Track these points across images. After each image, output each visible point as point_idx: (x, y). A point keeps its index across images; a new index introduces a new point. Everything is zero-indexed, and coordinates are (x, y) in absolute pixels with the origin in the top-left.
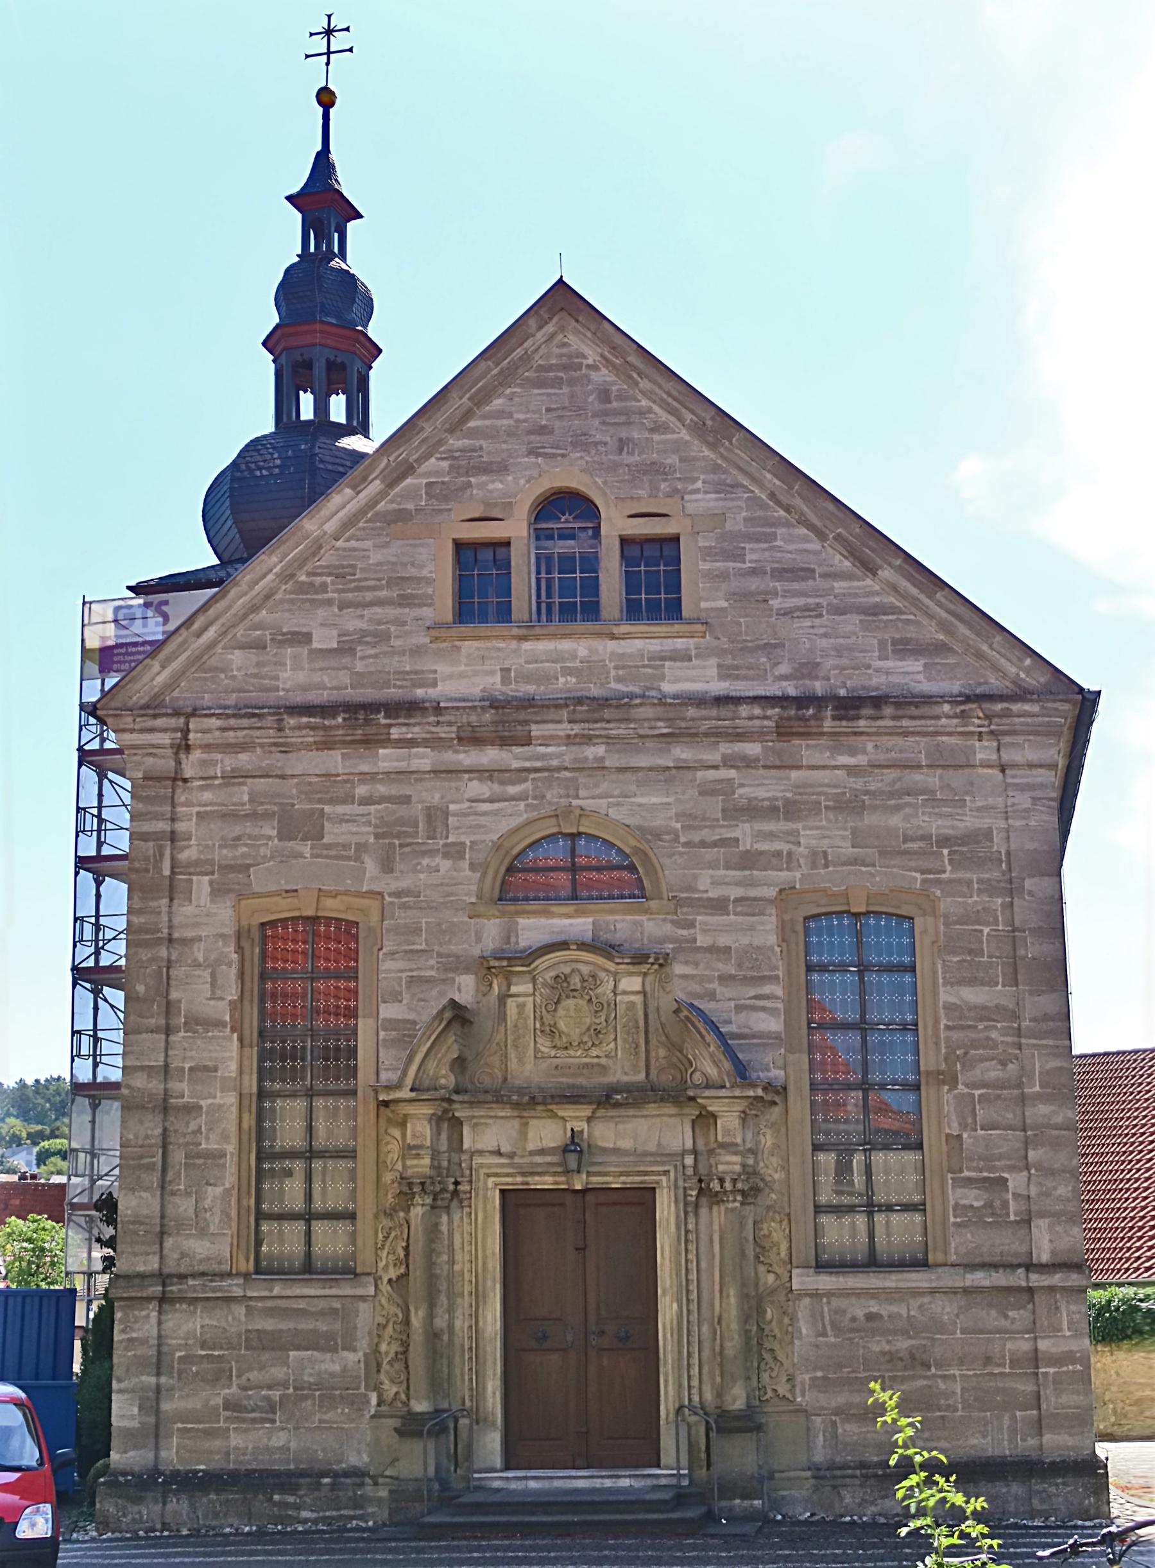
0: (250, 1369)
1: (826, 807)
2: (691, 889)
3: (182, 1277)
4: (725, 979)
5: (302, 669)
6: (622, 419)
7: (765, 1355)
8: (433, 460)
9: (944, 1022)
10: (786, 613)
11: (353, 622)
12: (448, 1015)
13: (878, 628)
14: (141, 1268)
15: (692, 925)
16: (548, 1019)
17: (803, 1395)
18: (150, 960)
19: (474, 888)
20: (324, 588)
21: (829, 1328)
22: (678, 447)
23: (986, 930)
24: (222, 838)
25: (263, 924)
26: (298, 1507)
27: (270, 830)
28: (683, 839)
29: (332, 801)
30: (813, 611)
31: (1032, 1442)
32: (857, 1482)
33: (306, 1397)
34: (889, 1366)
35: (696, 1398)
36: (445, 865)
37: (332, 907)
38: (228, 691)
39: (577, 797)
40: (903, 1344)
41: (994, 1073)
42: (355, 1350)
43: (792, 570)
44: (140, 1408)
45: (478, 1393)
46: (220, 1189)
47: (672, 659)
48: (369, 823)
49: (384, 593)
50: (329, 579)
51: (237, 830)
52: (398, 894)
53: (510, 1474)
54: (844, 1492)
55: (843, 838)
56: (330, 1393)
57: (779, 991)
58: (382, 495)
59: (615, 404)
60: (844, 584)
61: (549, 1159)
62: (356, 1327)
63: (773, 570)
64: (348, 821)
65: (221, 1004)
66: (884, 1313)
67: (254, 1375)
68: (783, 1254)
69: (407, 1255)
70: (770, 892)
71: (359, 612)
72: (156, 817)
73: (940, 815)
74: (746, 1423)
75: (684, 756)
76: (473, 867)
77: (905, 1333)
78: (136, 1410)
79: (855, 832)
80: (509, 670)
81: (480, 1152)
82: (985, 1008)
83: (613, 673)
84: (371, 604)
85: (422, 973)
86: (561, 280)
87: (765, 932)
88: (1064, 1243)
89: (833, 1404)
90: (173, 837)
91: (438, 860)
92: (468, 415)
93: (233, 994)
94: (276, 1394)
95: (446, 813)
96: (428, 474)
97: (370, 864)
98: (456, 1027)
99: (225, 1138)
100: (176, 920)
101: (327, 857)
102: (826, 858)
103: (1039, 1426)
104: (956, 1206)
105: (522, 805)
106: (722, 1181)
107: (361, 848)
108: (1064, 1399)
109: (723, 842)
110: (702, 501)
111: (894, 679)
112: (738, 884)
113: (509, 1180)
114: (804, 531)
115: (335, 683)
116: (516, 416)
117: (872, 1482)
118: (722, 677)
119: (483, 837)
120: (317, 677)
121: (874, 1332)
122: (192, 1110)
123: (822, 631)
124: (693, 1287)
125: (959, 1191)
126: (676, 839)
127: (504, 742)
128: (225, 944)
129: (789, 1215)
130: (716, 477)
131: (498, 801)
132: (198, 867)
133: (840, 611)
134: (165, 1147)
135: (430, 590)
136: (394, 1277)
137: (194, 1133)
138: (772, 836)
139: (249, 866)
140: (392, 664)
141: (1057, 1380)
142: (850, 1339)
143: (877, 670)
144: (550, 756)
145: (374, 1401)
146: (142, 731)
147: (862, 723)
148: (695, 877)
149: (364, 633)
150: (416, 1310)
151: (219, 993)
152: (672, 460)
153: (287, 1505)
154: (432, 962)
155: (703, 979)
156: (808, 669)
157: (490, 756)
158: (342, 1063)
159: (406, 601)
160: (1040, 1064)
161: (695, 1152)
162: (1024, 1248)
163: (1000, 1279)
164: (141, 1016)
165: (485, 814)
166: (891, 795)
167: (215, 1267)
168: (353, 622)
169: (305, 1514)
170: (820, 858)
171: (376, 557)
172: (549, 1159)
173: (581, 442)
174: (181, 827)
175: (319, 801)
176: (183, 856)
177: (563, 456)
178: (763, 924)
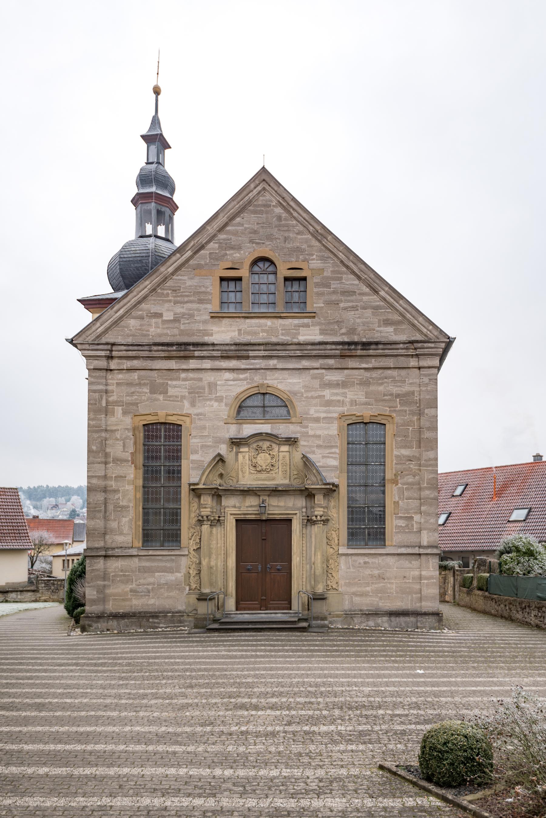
0: (140, 579)
2: (307, 414)
3: (113, 549)
4: (319, 446)
5: (159, 328)
6: (286, 228)
8: (212, 243)
9: (395, 462)
10: (345, 309)
11: (179, 309)
12: (218, 459)
13: (378, 315)
14: (97, 546)
15: (307, 427)
16: (254, 460)
18: (98, 437)
19: (226, 413)
20: (168, 295)
22: (307, 241)
23: (411, 428)
24: (127, 393)
25: (144, 425)
26: (159, 623)
27: (146, 390)
28: (305, 396)
29: (171, 380)
30: (355, 308)
31: (418, 605)
33: (162, 588)
35: (304, 589)
36: (216, 404)
37: (172, 419)
38: (128, 336)
39: (266, 379)
40: (376, 572)
41: (410, 479)
43: (348, 292)
44: (97, 592)
45: (226, 586)
46: (127, 519)
47: (303, 326)
48: (186, 388)
49: (192, 298)
50: (170, 292)
51: (133, 389)
52: (197, 415)
53: (238, 612)
54: (355, 619)
56: (170, 586)
57: (337, 451)
58: (191, 257)
59: (283, 222)
60: (367, 298)
61: (254, 509)
63: (341, 292)
65: (127, 454)
67: (142, 581)
68: (336, 541)
70: (336, 415)
71: (182, 305)
72: (99, 384)
73: (397, 386)
74: (321, 598)
75: (306, 364)
77: (377, 568)
78: (95, 593)
79: (367, 393)
80: (241, 330)
81: (228, 507)
82: (409, 457)
83: (280, 332)
84: (187, 302)
86: (263, 167)
87: (333, 429)
88: (432, 539)
90: (106, 392)
91: (213, 402)
92: (226, 225)
93: (132, 450)
94: (150, 587)
95: (216, 385)
96: (210, 249)
97: (186, 404)
98: (220, 463)
99: (130, 501)
100: (109, 423)
101: (169, 400)
103: (421, 600)
104: (396, 526)
105: (245, 382)
106: (316, 517)
107: (183, 397)
108: (429, 591)
110: (315, 264)
111: (383, 334)
112: (325, 412)
114: (352, 276)
115: (172, 333)
116: (245, 226)
118: (321, 334)
120: (165, 331)
122: (116, 491)
123: (358, 316)
124: (304, 552)
125: (397, 521)
126: (302, 396)
127: (239, 358)
128: (129, 432)
130: (321, 254)
131: (236, 380)
132: (117, 403)
133: (364, 308)
134: (105, 504)
135: (210, 297)
137: (117, 499)
138: (337, 394)
139: (138, 403)
140: (195, 327)
141: (427, 585)
143: (377, 331)
144: (256, 364)
145: (187, 588)
146: (92, 350)
147: (371, 351)
149: (184, 314)
151: (126, 450)
152: (304, 246)
153: (155, 623)
154: (210, 440)
155: (310, 447)
156: (352, 331)
157: (233, 364)
158: (176, 475)
159: (201, 301)
160: (427, 476)
161: (306, 507)
162: (418, 540)
163: (410, 551)
164: (94, 457)
165: (231, 385)
166: (380, 379)
167: (126, 545)
168: (179, 309)
169: (161, 625)
170: (353, 403)
171: (189, 283)
172: (254, 509)
173: (270, 237)
174: (110, 388)
175: (166, 379)
176: (111, 399)
177: (263, 243)
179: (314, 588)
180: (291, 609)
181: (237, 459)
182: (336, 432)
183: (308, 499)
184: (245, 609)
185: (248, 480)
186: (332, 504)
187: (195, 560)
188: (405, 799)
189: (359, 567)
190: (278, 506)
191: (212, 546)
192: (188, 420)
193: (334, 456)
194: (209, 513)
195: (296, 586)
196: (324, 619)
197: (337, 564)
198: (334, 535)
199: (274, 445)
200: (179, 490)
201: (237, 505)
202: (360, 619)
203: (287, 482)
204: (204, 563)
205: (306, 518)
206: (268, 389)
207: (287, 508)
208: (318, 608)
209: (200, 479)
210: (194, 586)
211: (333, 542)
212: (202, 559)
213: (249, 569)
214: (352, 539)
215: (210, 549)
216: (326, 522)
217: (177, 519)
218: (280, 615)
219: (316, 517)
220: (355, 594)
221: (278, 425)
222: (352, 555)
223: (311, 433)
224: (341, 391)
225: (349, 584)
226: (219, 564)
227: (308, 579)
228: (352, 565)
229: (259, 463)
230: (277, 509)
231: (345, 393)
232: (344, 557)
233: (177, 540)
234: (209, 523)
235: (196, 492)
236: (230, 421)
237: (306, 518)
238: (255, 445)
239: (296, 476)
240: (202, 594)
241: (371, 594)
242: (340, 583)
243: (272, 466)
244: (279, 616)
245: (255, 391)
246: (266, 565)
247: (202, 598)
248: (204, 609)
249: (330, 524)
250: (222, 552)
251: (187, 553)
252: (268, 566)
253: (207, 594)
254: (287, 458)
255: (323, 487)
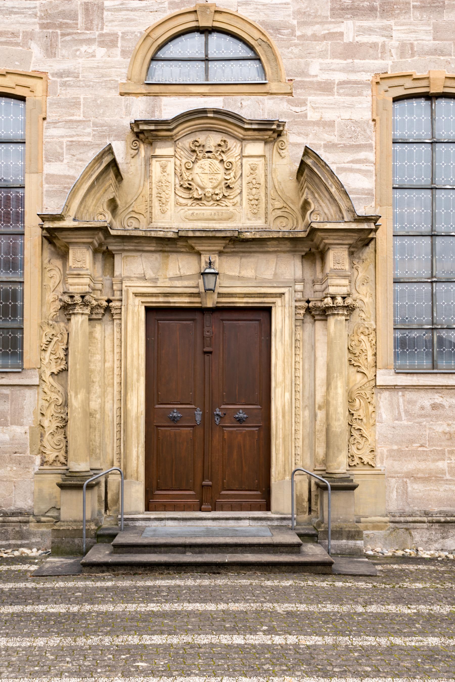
1: (414, 7)
2: (303, 73)
7: (354, 433)
15: (303, 103)
17: (382, 462)
19: (125, 71)
21: (403, 414)
28: (298, 33)
32: (425, 526)
34: (449, 443)
36: (101, 52)
42: (22, 425)
45: (123, 455)
52: (60, 75)
53: (153, 515)
54: (414, 533)
55: (426, 32)
57: (371, 156)
62: (23, 408)
64: (16, 13)
66: (446, 404)
68: (370, 358)
69: (66, 355)
70: (367, 77)
76: (124, 53)
79: (436, 29)
81: (129, 278)
85: (80, 139)
87: (362, 108)
89: (405, 469)
95: (101, 8)
97: (36, 50)
102: (412, 48)
106: (333, 298)
107: (29, 36)
109: (331, 36)
112: (343, 70)
113: (154, 299)
117: (437, 526)
119: (134, 29)
121: (437, 417)
126: (293, 33)
129: (375, 330)
136: (55, 371)
138: (370, 30)
142: (420, 423)
145: (38, 460)
148: (307, 64)
150: (76, 394)
154: (89, 130)
170: (406, 49)
172: (186, 283)
178: (360, 103)
179: (325, 461)
180: (268, 508)
181: (148, 174)
182: (368, 116)
183: (307, 265)
184: (165, 508)
185: (173, 217)
186: (361, 273)
187: (54, 396)
188: (243, 642)
189: (421, 416)
190: (240, 278)
191: (92, 367)
192: (38, 85)
193: (363, 167)
194: (87, 289)
195: (281, 457)
196: (355, 535)
197: (371, 408)
198: (366, 345)
199: (231, 143)
200: (19, 241)
201: (150, 274)
202: (426, 535)
203: (260, 223)
204: (76, 402)
205: (304, 304)
206: (218, 17)
207: (263, 283)
208: (339, 509)
209: (67, 206)
210: (51, 455)
211: (362, 359)
212: (71, 394)
213: (174, 419)
214: (403, 353)
215: (89, 373)
216: (350, 309)
217: (15, 307)
218: (247, 523)
219: (333, 298)
220: (412, 476)
221: (239, 98)
222: (405, 388)
223: (312, 116)
224: (377, 23)
225: (398, 455)
226: (108, 406)
227: (307, 441)
228: (406, 412)
229: (197, 179)
230: (238, 283)
231: (388, 28)
232: (386, 394)
233: (14, 354)
234: (87, 311)
235: (56, 239)
236: (132, 88)
237: (304, 304)
238: (187, 142)
239: (279, 213)
240: (70, 474)
241: (448, 477)
242: (378, 451)
243: (228, 187)
244: (245, 526)
245: (188, 22)
246: (212, 409)
247: (72, 483)
248: (75, 509)
249: (356, 317)
250: (116, 380)
251: (36, 381)
252: (218, 412)
253: (81, 476)
254: (260, 172)
255: (354, 226)
